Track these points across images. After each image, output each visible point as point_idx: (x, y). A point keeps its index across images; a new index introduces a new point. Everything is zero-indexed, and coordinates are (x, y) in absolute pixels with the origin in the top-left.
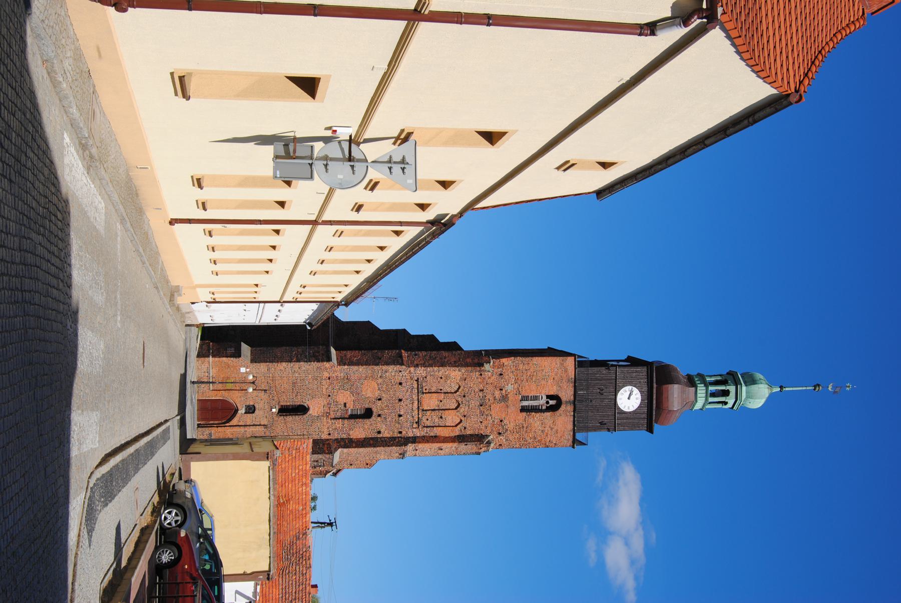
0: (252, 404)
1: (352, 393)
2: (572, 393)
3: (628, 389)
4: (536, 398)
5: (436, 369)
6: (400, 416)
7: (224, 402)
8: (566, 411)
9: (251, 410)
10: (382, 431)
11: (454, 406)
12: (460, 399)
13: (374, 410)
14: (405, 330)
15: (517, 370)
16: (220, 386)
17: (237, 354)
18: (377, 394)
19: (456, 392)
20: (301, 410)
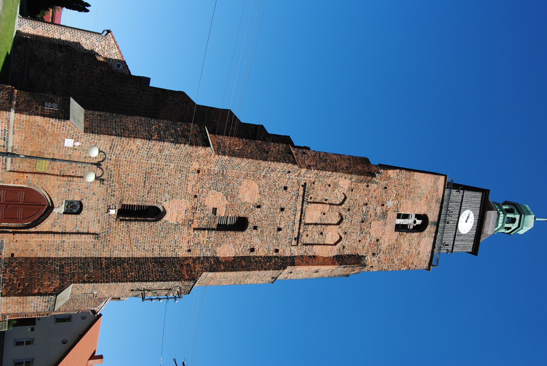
0: (77, 198)
1: (226, 195)
4: (406, 216)
5: (328, 173)
7: (29, 192)
8: (430, 232)
9: (75, 208)
10: (256, 248)
11: (336, 220)
12: (343, 213)
13: (251, 220)
14: (262, 126)
15: (399, 184)
16: (25, 166)
17: (64, 114)
18: (256, 199)
19: (341, 204)
20: (153, 214)
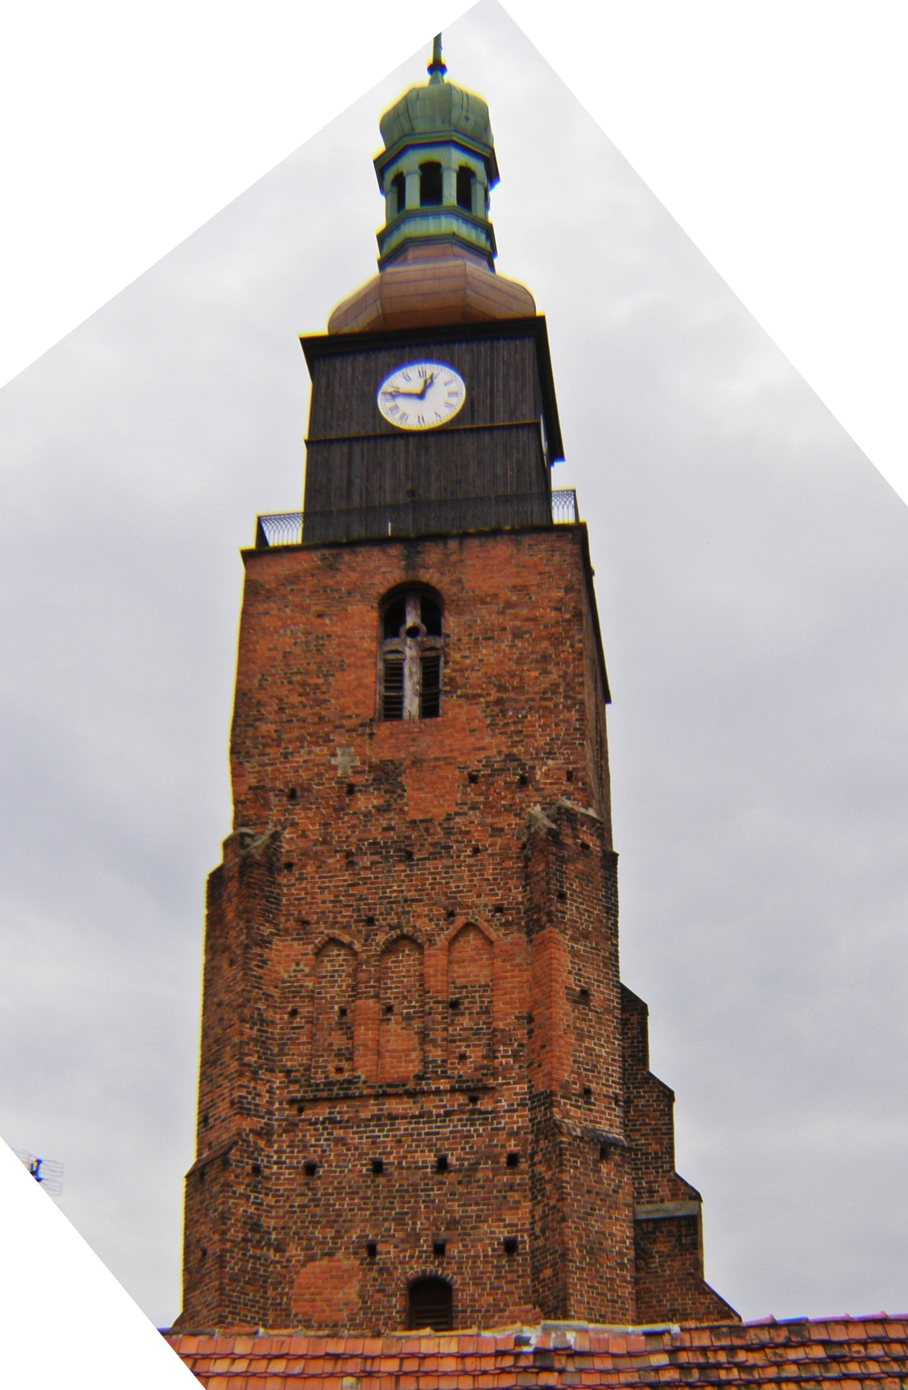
2: (376, 552)
3: (384, 405)
6: (442, 1165)
10: (503, 1234)
12: (381, 938)
13: (415, 1269)
18: (347, 1261)
